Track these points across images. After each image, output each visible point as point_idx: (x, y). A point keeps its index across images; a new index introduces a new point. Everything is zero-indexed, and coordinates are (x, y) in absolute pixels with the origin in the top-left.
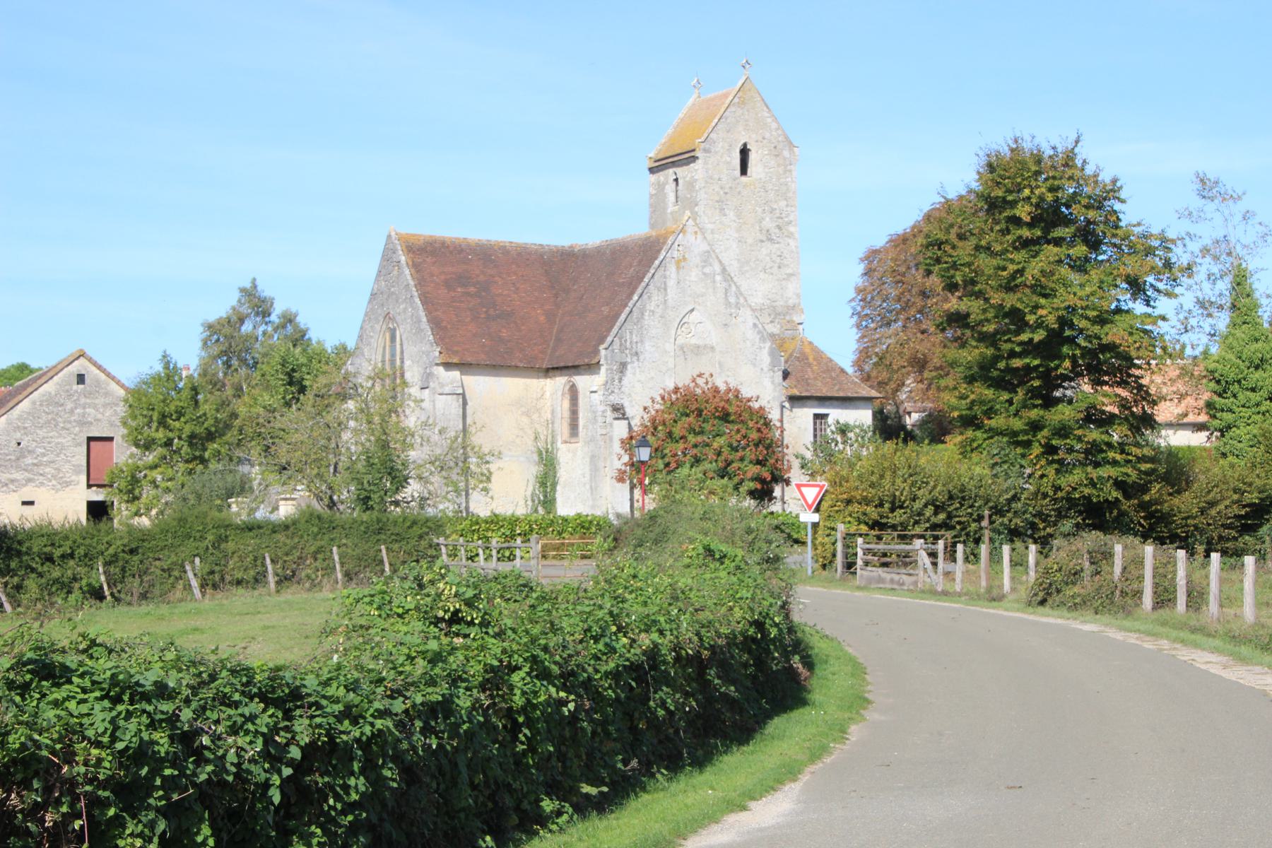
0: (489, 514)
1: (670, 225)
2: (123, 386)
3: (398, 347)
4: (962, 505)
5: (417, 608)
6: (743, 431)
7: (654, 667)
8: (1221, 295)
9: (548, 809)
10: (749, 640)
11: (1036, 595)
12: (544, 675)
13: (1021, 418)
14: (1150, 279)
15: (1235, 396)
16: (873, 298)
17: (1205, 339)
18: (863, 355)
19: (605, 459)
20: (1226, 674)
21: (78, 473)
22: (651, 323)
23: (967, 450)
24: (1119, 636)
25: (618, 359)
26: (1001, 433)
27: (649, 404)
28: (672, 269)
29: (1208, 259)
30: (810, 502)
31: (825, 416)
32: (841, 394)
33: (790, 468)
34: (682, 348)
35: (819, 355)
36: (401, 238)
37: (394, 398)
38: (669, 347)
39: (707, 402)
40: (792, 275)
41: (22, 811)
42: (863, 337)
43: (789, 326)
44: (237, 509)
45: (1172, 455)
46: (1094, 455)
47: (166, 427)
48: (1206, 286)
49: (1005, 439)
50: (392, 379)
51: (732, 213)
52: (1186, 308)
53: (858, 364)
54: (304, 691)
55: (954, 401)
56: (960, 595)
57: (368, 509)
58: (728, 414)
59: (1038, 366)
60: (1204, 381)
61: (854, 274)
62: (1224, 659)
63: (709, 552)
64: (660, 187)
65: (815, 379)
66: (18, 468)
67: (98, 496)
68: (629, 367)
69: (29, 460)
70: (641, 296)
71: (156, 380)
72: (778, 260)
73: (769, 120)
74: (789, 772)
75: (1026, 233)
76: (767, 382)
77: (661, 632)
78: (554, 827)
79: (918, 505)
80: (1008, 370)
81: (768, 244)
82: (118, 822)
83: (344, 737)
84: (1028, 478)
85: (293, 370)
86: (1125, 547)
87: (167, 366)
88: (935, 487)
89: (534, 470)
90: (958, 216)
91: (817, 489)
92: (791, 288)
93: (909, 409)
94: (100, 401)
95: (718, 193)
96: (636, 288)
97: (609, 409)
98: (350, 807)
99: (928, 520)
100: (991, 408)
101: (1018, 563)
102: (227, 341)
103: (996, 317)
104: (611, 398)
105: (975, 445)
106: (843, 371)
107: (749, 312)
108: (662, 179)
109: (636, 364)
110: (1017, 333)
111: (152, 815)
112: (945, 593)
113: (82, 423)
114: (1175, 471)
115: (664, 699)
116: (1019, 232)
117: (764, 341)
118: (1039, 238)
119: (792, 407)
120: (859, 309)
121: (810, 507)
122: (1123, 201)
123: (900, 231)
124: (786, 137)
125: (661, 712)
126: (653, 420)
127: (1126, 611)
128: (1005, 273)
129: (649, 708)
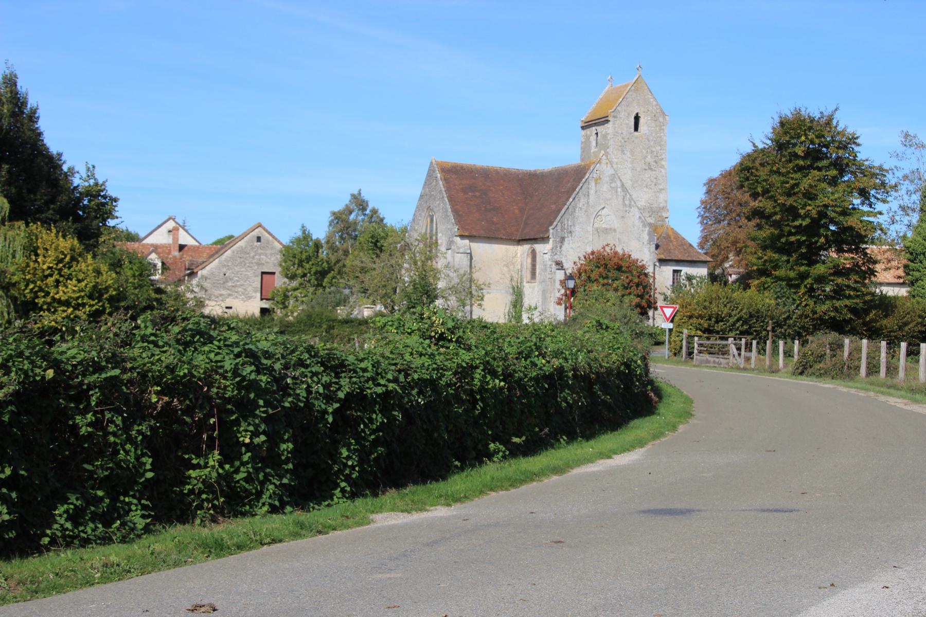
1: (593, 159)
2: (281, 244)
5: (419, 330)
6: (630, 278)
7: (560, 378)
8: (914, 203)
9: (492, 449)
10: (620, 374)
11: (798, 369)
12: (494, 374)
14: (873, 192)
15: (921, 262)
17: (904, 228)
18: (704, 240)
20: (905, 407)
21: (256, 292)
22: (580, 215)
23: (762, 288)
24: (845, 390)
26: (781, 279)
27: (577, 260)
29: (907, 182)
34: (597, 229)
35: (677, 236)
36: (438, 163)
37: (430, 251)
38: (590, 229)
40: (661, 189)
41: (181, 409)
42: (704, 229)
44: (341, 312)
45: (883, 298)
46: (838, 293)
47: (302, 267)
48: (906, 197)
50: (431, 244)
52: (893, 210)
53: (701, 246)
54: (346, 363)
55: (754, 260)
56: (753, 370)
58: (622, 267)
59: (804, 241)
60: (903, 253)
61: (700, 194)
62: (906, 401)
63: (600, 324)
64: (588, 138)
66: (225, 288)
67: (266, 305)
69: (230, 284)
71: (298, 241)
74: (641, 443)
75: (801, 163)
76: (646, 251)
77: (566, 359)
78: (495, 459)
79: (732, 320)
82: (237, 422)
83: (369, 391)
84: (797, 305)
85: (377, 241)
86: (851, 341)
87: (304, 232)
88: (741, 310)
89: (510, 298)
92: (662, 197)
94: (269, 252)
96: (571, 195)
97: (554, 264)
98: (374, 432)
99: (737, 329)
101: (788, 354)
102: (341, 222)
106: (691, 245)
107: (636, 210)
110: (793, 221)
111: (257, 421)
112: (745, 369)
113: (259, 264)
114: (886, 305)
115: (566, 397)
116: (797, 162)
118: (809, 166)
121: (668, 319)
122: (859, 145)
123: (728, 169)
124: (662, 110)
125: (564, 404)
126: (579, 270)
127: (850, 377)
129: (557, 401)
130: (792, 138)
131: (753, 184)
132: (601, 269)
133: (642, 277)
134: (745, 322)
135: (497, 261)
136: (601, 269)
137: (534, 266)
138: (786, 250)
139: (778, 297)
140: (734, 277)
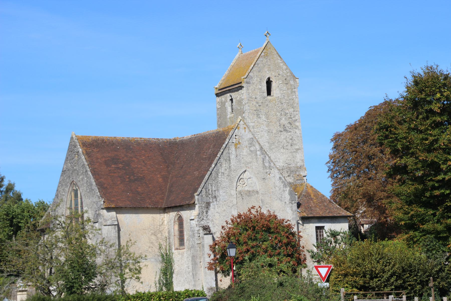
0: (135, 293)
3: (79, 200)
4: (411, 275)
6: (279, 238)
13: (441, 224)
16: (339, 161)
18: (336, 192)
19: (200, 257)
23: (411, 242)
25: (205, 200)
27: (225, 224)
28: (233, 149)
30: (323, 276)
31: (323, 228)
32: (331, 215)
33: (305, 259)
34: (240, 193)
35: (316, 193)
38: (233, 192)
39: (257, 222)
42: (335, 183)
43: (298, 178)
49: (167, 235)
51: (264, 117)
57: (72, 293)
58: (270, 228)
61: (327, 149)
64: (223, 104)
65: (315, 207)
68: (211, 204)
70: (216, 164)
72: (291, 141)
73: (281, 64)
75: (438, 119)
76: (289, 210)
79: (386, 276)
80: (432, 197)
81: (285, 133)
85: (13, 218)
88: (394, 265)
90: (396, 112)
91: (327, 269)
92: (299, 156)
93: (362, 223)
95: (255, 106)
97: (201, 229)
100: (423, 219)
103: (422, 167)
104: (202, 222)
105: (415, 239)
107: (276, 171)
108: (223, 99)
109: (215, 203)
117: (286, 187)
119: (303, 223)
120: (332, 167)
121: (323, 279)
123: (353, 123)
124: (292, 73)
128: (427, 142)
130: (427, 95)
131: (393, 142)
132: (250, 232)
133: (291, 236)
134: (399, 277)
135: (145, 230)
136: (250, 232)
137: (181, 232)
138: (433, 203)
139: (428, 250)
140: (366, 226)
